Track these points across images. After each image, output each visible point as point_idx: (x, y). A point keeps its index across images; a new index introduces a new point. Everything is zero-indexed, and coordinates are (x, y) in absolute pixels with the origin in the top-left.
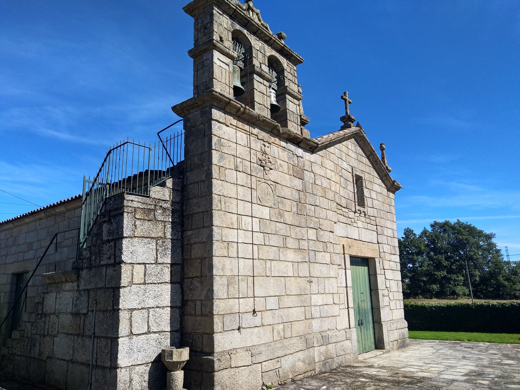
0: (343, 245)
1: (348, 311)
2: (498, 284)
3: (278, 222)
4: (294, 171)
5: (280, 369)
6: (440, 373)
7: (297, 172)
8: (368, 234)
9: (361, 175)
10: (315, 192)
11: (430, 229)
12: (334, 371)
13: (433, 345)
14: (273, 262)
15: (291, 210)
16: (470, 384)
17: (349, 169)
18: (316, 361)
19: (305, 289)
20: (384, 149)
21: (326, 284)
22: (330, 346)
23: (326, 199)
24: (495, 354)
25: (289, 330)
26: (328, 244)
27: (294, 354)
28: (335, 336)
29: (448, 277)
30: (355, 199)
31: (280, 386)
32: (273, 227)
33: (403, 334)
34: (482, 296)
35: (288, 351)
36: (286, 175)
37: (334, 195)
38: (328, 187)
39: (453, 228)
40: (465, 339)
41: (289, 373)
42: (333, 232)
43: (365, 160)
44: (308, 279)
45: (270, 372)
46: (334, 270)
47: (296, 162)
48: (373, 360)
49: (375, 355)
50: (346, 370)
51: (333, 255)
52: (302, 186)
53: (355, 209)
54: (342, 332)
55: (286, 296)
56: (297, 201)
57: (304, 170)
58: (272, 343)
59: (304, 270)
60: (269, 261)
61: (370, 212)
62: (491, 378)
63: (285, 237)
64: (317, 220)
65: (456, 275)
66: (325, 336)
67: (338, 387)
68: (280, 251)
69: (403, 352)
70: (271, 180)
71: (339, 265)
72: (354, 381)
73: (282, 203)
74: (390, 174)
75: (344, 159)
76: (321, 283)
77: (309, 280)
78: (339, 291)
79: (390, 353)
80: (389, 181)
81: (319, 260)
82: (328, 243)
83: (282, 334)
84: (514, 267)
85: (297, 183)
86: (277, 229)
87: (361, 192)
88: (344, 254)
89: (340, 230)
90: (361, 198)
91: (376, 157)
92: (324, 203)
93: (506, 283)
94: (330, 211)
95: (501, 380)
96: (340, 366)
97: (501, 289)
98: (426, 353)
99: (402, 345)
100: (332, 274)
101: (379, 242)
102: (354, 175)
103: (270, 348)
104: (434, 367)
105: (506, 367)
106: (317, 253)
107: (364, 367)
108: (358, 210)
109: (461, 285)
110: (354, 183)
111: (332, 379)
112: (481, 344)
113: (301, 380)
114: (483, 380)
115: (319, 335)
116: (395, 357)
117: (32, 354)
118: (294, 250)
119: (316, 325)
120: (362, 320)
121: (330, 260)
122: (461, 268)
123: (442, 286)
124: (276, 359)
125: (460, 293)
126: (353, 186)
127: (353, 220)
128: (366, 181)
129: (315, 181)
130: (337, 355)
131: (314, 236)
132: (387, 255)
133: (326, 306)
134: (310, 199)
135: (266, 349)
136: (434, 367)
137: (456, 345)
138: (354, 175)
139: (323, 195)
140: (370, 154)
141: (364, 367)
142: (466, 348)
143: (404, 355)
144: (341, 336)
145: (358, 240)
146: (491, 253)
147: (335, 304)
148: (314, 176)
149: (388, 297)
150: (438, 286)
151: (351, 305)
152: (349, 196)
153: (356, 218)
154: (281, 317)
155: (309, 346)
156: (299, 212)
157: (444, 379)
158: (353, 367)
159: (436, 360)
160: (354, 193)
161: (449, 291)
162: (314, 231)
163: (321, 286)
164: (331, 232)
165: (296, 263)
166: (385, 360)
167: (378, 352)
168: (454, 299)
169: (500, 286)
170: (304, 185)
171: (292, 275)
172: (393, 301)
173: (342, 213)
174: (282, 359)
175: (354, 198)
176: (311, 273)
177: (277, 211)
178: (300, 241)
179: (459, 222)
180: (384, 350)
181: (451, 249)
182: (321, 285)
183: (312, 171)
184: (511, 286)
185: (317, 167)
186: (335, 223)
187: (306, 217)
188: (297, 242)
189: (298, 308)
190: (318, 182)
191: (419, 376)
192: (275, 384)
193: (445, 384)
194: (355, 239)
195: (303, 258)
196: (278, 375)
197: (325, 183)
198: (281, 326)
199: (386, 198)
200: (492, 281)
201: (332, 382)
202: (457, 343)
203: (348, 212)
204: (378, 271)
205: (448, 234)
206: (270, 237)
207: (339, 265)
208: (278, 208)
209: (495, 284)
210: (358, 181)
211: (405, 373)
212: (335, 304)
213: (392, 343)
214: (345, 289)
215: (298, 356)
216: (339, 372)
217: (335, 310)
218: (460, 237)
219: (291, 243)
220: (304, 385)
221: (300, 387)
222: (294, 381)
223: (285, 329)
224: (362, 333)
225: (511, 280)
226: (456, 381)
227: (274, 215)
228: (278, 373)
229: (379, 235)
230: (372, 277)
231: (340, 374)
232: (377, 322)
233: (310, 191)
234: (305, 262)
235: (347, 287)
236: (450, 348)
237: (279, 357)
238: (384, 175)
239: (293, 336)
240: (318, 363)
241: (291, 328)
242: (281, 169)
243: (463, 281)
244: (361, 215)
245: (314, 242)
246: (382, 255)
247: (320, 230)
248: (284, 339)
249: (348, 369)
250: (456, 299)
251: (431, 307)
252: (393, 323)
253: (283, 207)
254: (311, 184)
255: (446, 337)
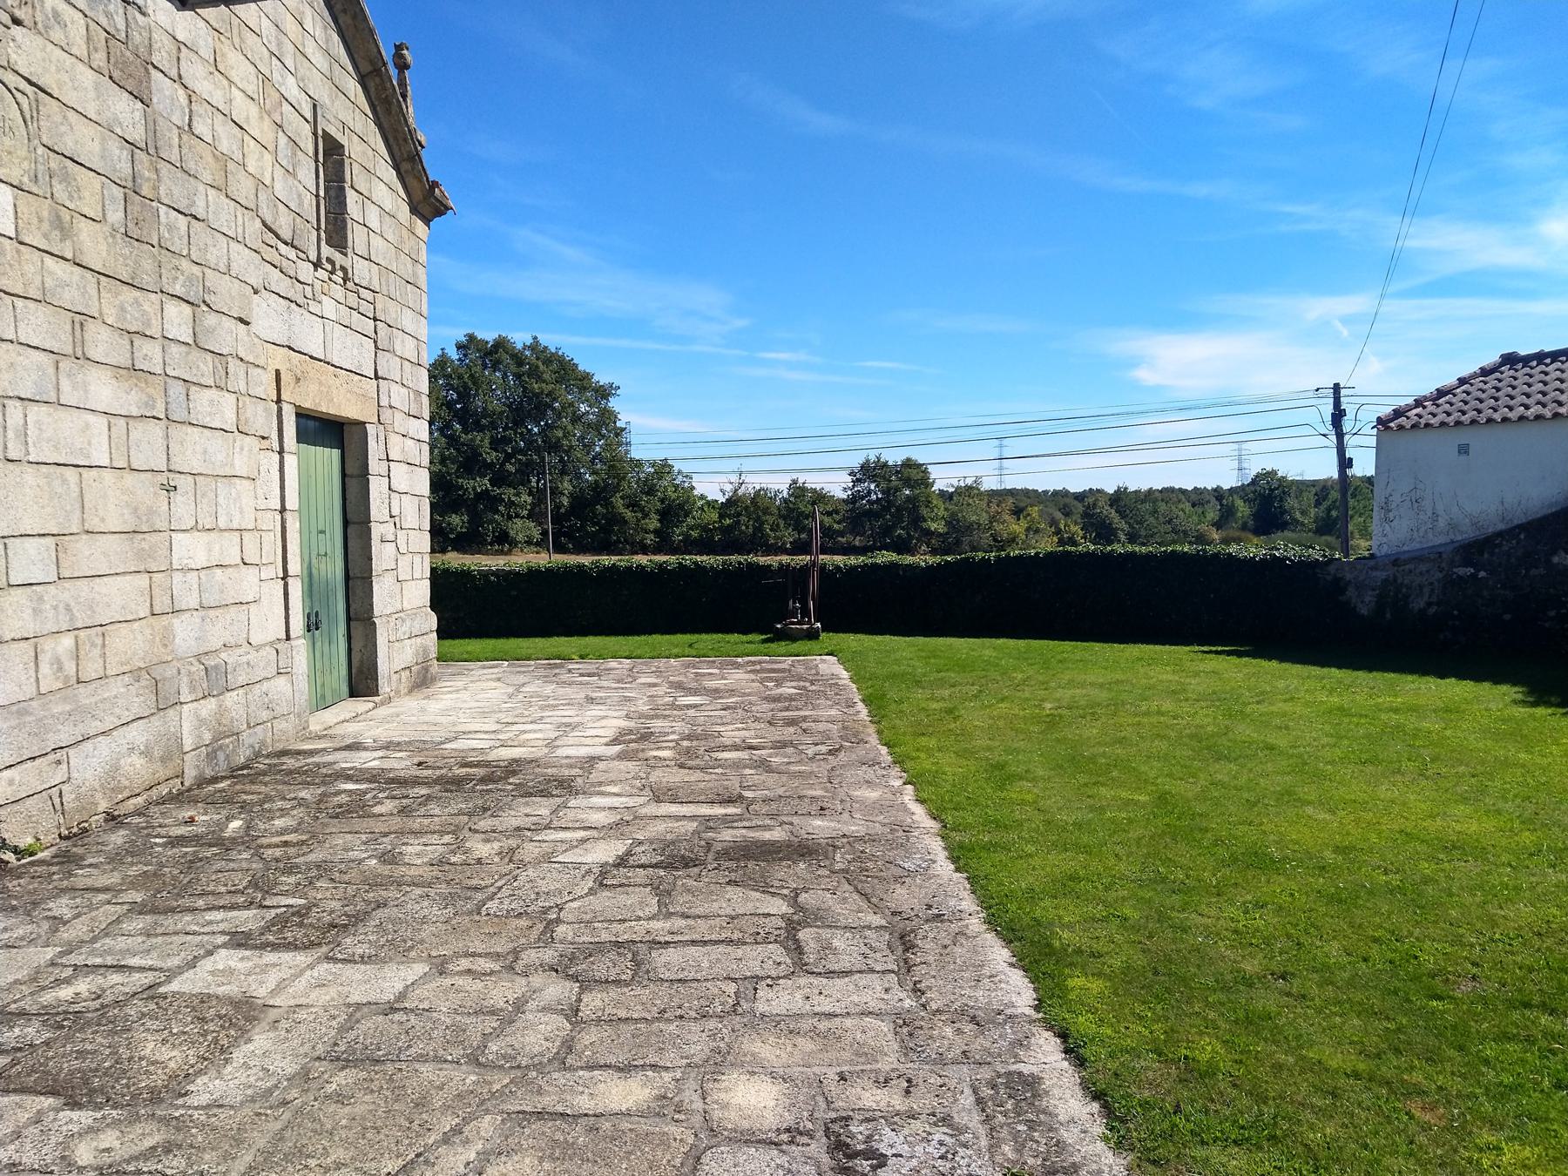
0: (278, 373)
1: (286, 586)
2: (610, 516)
3: (52, 254)
4: (112, 61)
5: (65, 788)
6: (551, 744)
7: (123, 65)
8: (349, 343)
9: (343, 140)
10: (191, 165)
11: (454, 354)
12: (245, 772)
13: (500, 675)
14: (34, 410)
15: (104, 215)
16: (634, 763)
17: (304, 105)
18: (186, 748)
19: (151, 512)
20: (407, 66)
21: (221, 500)
22: (230, 699)
23: (227, 201)
24: (655, 685)
25: (97, 651)
26: (233, 365)
27: (115, 733)
28: (246, 666)
29: (492, 493)
30: (318, 220)
31: (64, 844)
32: (30, 269)
33: (425, 650)
34: (571, 546)
35: (93, 725)
36: (80, 64)
37: (254, 191)
38: (238, 156)
39: (518, 358)
40: (574, 653)
41: (99, 796)
42: (247, 323)
43: (353, 87)
44: (162, 478)
45: (29, 801)
46: (245, 452)
47: (121, 25)
48: (351, 728)
49: (354, 715)
50: (283, 764)
51: (244, 402)
52: (143, 128)
53: (319, 254)
54: (265, 654)
55: (84, 536)
56: (123, 183)
57: (150, 67)
58: (34, 704)
59: (148, 444)
60: (18, 403)
61: (362, 271)
62: (671, 741)
63: (80, 319)
64: (196, 270)
65: (514, 489)
66: (216, 667)
67: (282, 816)
68: (61, 369)
69: (428, 697)
70: (16, 68)
71: (263, 438)
72: (324, 795)
73: (66, 178)
74: (423, 153)
75: (289, 63)
76: (203, 495)
77: (165, 483)
78: (259, 521)
79: (392, 704)
80: (420, 181)
81: (200, 417)
82: (230, 359)
83: (70, 668)
84: (648, 474)
85: (124, 109)
86: (49, 283)
87: (337, 197)
88: (279, 401)
89: (269, 318)
90: (336, 219)
91: (388, 85)
92: (222, 213)
93: (628, 514)
94: (241, 247)
95: (695, 743)
96: (258, 754)
97: (616, 528)
98: (489, 695)
99: (422, 681)
100: (241, 467)
101: (380, 374)
102: (320, 132)
103: (29, 719)
104: (530, 732)
105: (691, 712)
106: (193, 389)
107: (336, 750)
108: (328, 260)
109: (523, 517)
110: (317, 161)
111: (250, 797)
112: (613, 664)
113: (138, 813)
114: (658, 748)
115: (197, 664)
116: (413, 715)
117: (130, 859)
118: (114, 369)
119: (185, 633)
120: (317, 613)
121: (234, 419)
122: (526, 470)
123: (475, 520)
124: (52, 757)
125: (520, 537)
126: (313, 171)
127: (308, 289)
128: (354, 164)
129: (190, 120)
130: (248, 724)
131: (184, 327)
132: (399, 416)
133: (218, 571)
134: (172, 187)
135: (14, 722)
136: (530, 732)
137: (557, 671)
138: (320, 132)
139: (220, 182)
140: (371, 72)
141: (336, 750)
142: (582, 675)
143: (434, 706)
144: (262, 665)
145: (320, 360)
146: (603, 436)
147: (245, 564)
148: (187, 101)
149: (394, 544)
150: (466, 518)
151: (295, 567)
152: (301, 204)
153: (318, 284)
154: (68, 609)
155: (164, 703)
156: (135, 233)
157: (567, 757)
158: (299, 753)
159: (526, 713)
160: (317, 196)
161: (493, 532)
162: (187, 309)
163: (205, 506)
164: (241, 320)
165: (122, 421)
166: (387, 726)
167: (361, 705)
168: (501, 552)
169: (615, 520)
170: (151, 125)
171: (106, 462)
172: (405, 557)
173: (276, 259)
174: (71, 752)
175: (315, 214)
176: (173, 459)
177: (45, 208)
178: (138, 341)
179: (535, 346)
180: (376, 699)
181: (507, 417)
182: (205, 501)
183: (180, 76)
184: (638, 520)
185: (200, 67)
186: (256, 292)
187: (156, 253)
188: (126, 342)
189: (128, 577)
190: (200, 128)
191: (502, 758)
192: (45, 840)
193: (578, 770)
194: (311, 357)
195: (146, 404)
196: (58, 807)
197: (227, 140)
198: (67, 641)
199: (405, 232)
200: (598, 507)
201: (253, 804)
202: (556, 666)
203: (295, 259)
204: (375, 465)
205: (505, 376)
206: (18, 311)
207: (263, 438)
208: (49, 195)
209: (604, 516)
210: (331, 154)
211: (463, 754)
212: (245, 564)
213: (397, 676)
214: (278, 517)
215: (130, 737)
216: (264, 773)
217: (248, 583)
218: (536, 386)
219: (101, 343)
220: (160, 826)
221: (149, 835)
222: (114, 818)
223: (82, 652)
224: (318, 654)
225: (639, 506)
226: (600, 758)
227: (35, 221)
228: (57, 801)
229: (379, 352)
230: (350, 482)
231: (267, 779)
232: (360, 618)
233: (175, 158)
234: (154, 417)
235: (283, 510)
236: (546, 680)
237: (62, 748)
238: (405, 156)
239: (109, 672)
240: (193, 753)
241: (104, 645)
242: (57, 35)
243: (529, 507)
244: (334, 277)
245: (184, 348)
246: (386, 415)
247: (205, 308)
248: (76, 686)
249: (284, 759)
250: (506, 554)
251: (485, 575)
252: (403, 621)
253: (71, 198)
254: (176, 131)
255: (524, 652)
